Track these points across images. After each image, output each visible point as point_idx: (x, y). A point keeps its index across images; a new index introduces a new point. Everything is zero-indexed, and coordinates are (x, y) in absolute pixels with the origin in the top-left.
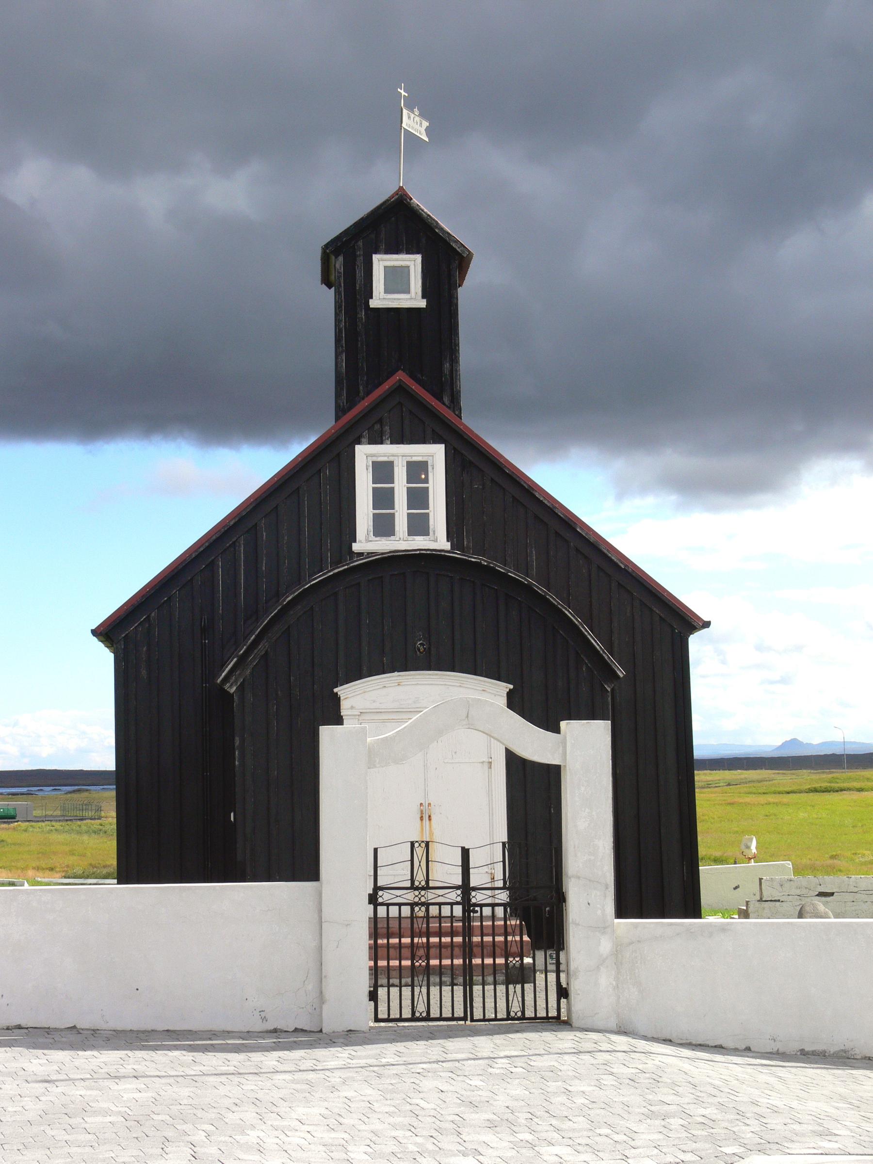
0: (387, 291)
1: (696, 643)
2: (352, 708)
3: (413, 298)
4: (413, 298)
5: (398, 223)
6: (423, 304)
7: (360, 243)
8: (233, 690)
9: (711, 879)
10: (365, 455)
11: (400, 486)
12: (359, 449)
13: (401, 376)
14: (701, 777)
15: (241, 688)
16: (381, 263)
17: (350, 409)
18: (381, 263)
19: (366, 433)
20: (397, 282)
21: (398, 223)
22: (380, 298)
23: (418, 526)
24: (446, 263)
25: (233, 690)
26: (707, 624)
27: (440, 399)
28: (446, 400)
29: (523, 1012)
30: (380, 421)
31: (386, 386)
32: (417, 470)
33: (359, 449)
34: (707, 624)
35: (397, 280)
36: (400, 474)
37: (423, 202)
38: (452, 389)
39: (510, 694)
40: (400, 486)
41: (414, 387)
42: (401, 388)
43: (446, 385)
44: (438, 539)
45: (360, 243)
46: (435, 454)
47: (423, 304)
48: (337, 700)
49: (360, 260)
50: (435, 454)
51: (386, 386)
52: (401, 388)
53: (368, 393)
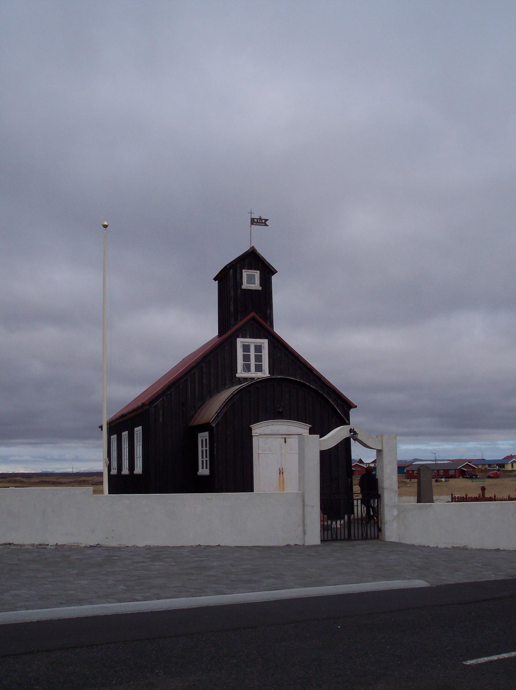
0: (247, 283)
1: (352, 412)
2: (256, 433)
3: (256, 286)
4: (256, 286)
5: (252, 259)
6: (260, 288)
7: (239, 265)
8: (214, 425)
9: (435, 498)
10: (240, 342)
11: (252, 353)
12: (238, 339)
13: (253, 314)
14: (297, 452)
15: (217, 425)
16: (245, 273)
17: (236, 324)
18: (245, 273)
19: (240, 334)
20: (251, 280)
21: (252, 259)
22: (245, 286)
23: (259, 368)
24: (267, 272)
25: (214, 425)
26: (356, 407)
27: (266, 322)
28: (268, 323)
29: (336, 536)
30: (246, 330)
31: (248, 318)
32: (258, 349)
33: (238, 339)
34: (356, 407)
35: (251, 279)
36: (252, 349)
37: (262, 252)
38: (270, 320)
39: (310, 429)
40: (252, 353)
41: (258, 318)
42: (253, 319)
43: (268, 317)
44: (265, 373)
45: (239, 265)
46: (265, 343)
47: (260, 288)
48: (251, 430)
49: (238, 271)
50: (265, 343)
51: (248, 318)
52: (253, 319)
53: (241, 320)
